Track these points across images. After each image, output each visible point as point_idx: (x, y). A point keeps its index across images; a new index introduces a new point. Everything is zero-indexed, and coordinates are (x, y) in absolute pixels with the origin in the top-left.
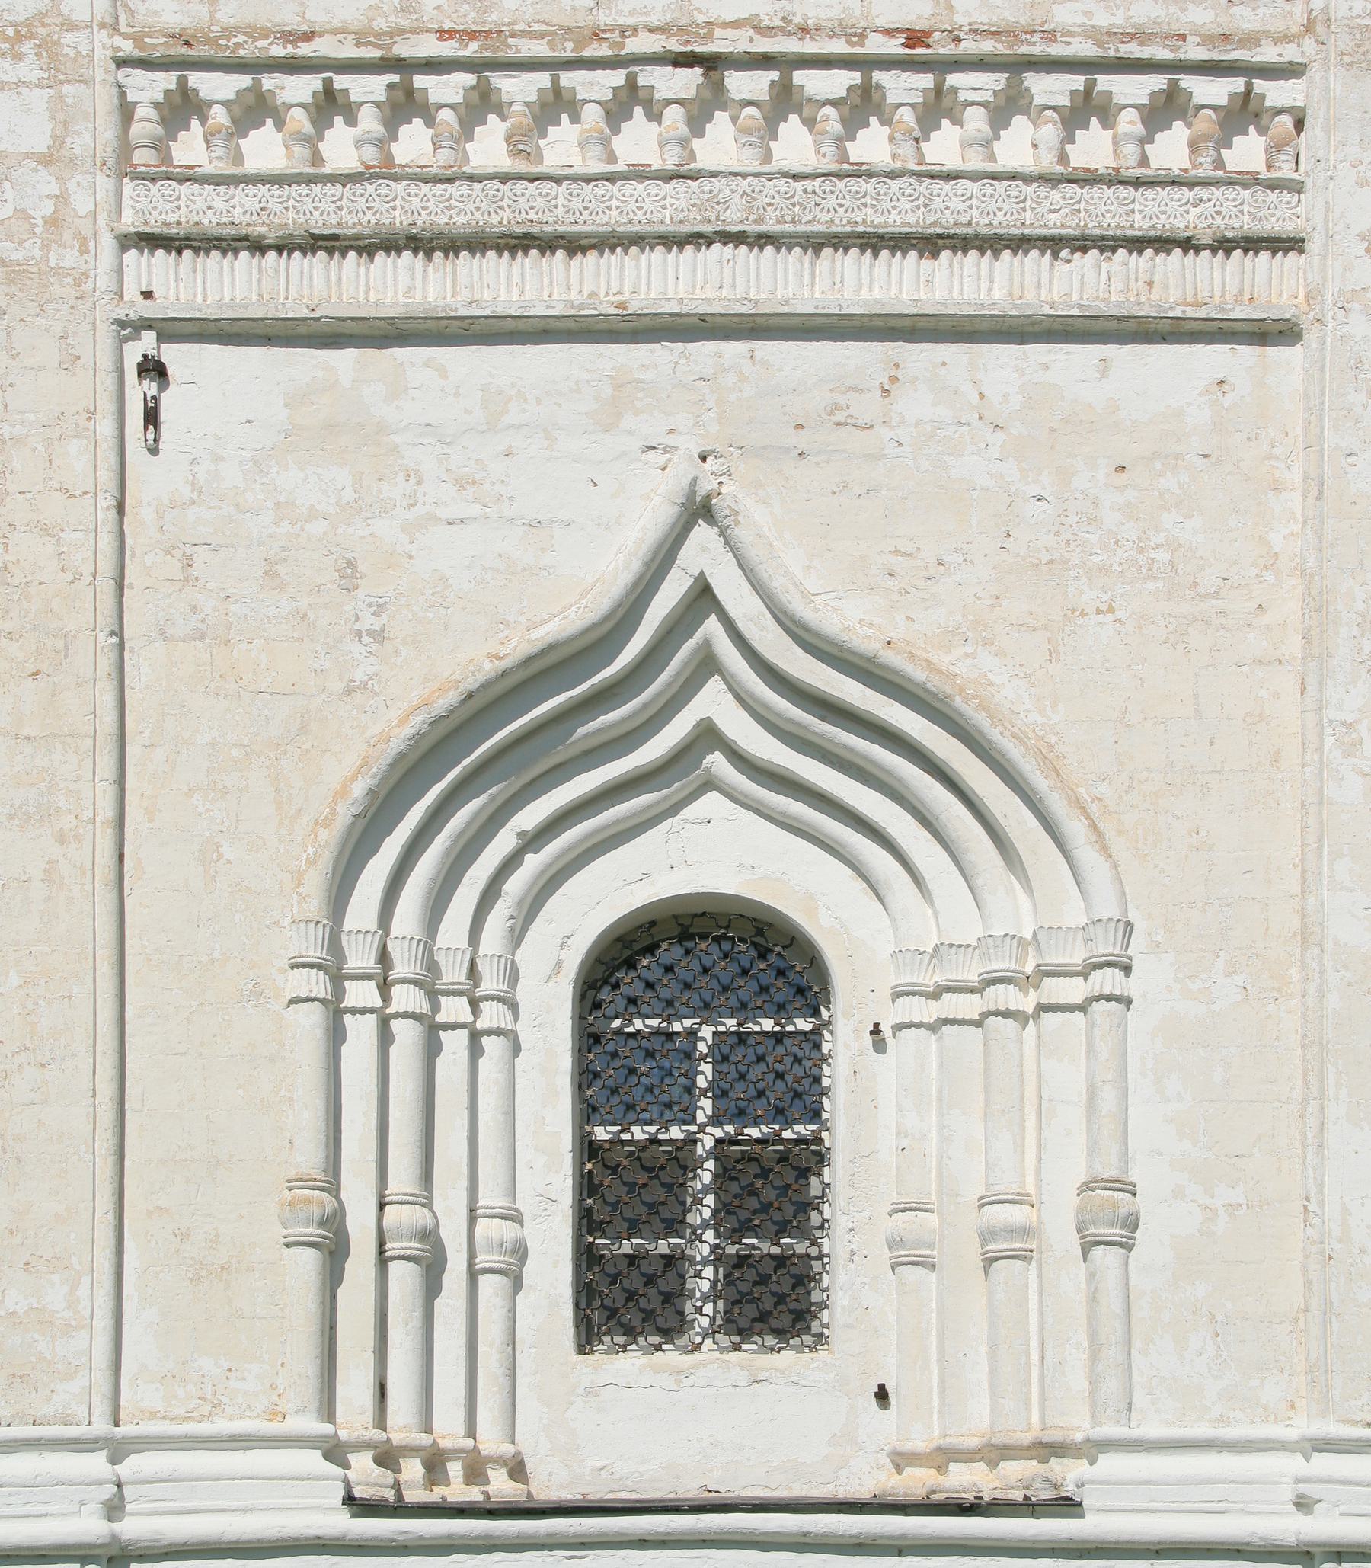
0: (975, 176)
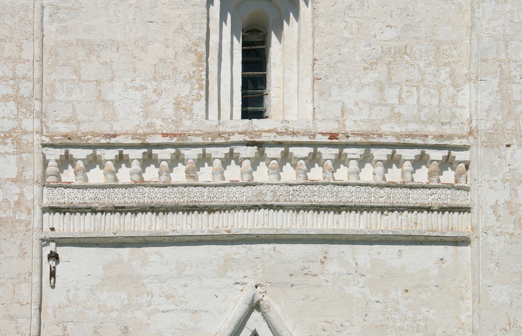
0: (353, 185)
